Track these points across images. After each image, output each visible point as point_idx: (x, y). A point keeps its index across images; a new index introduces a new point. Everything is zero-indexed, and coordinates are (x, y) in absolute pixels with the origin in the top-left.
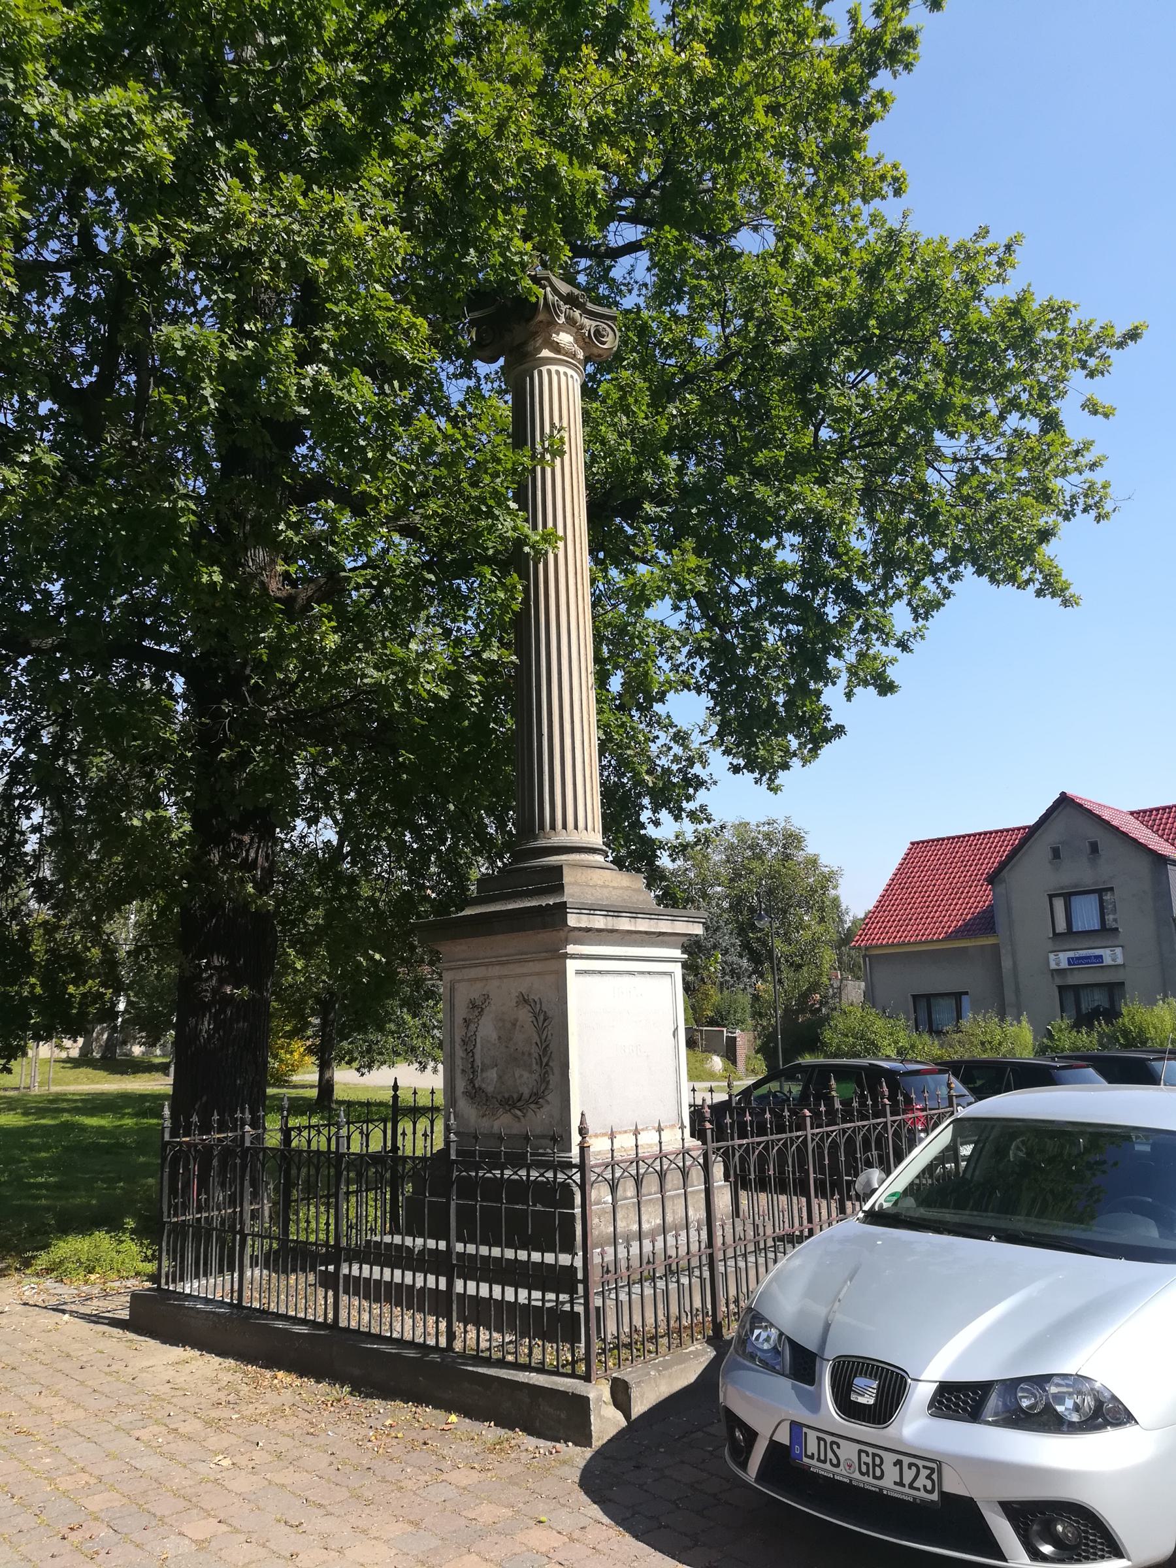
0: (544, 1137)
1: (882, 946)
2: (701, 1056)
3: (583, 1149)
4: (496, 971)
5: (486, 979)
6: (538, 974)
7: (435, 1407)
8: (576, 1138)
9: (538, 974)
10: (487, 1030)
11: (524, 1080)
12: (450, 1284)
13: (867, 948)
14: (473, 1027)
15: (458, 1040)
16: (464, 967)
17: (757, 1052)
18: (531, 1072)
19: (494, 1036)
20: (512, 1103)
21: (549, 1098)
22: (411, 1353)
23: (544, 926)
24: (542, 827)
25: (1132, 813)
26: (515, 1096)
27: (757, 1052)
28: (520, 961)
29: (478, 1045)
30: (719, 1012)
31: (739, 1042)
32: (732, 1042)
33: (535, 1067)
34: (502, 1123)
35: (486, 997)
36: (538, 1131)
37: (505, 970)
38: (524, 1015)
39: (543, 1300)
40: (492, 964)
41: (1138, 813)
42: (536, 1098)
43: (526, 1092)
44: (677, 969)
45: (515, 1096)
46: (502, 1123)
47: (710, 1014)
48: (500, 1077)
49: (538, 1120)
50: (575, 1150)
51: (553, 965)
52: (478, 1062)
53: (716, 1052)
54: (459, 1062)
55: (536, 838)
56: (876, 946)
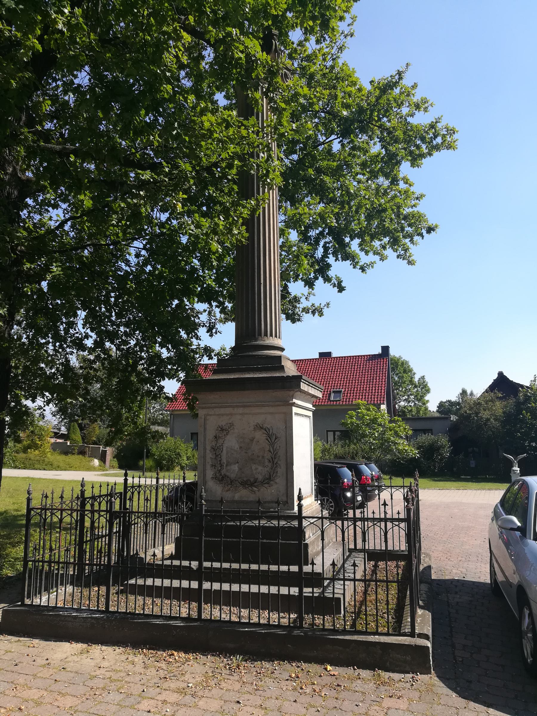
0: (272, 502)
1: (180, 410)
2: (87, 459)
3: (300, 506)
4: (240, 410)
5: (231, 414)
6: (271, 413)
7: (186, 652)
8: (296, 503)
9: (271, 413)
10: (231, 442)
11: (259, 471)
12: (200, 585)
13: (172, 411)
14: (220, 441)
15: (208, 448)
16: (216, 407)
17: (114, 458)
18: (264, 467)
19: (237, 446)
20: (249, 484)
21: (277, 480)
22: (279, 632)
23: (283, 388)
24: (260, 334)
25: (292, 361)
26: (252, 480)
27: (114, 458)
28: (258, 406)
29: (225, 451)
30: (98, 438)
31: (108, 453)
32: (104, 453)
33: (267, 463)
34: (242, 494)
35: (232, 425)
36: (269, 498)
37: (247, 410)
38: (260, 436)
39: (313, 593)
40: (237, 407)
41: (295, 361)
42: (268, 480)
43: (260, 478)
44: (310, 414)
45: (252, 480)
46: (242, 494)
47: (94, 439)
48: (240, 469)
49: (268, 493)
50: (296, 508)
51: (283, 409)
52: (224, 461)
53: (95, 457)
54: (208, 460)
55: (256, 340)
56: (177, 410)
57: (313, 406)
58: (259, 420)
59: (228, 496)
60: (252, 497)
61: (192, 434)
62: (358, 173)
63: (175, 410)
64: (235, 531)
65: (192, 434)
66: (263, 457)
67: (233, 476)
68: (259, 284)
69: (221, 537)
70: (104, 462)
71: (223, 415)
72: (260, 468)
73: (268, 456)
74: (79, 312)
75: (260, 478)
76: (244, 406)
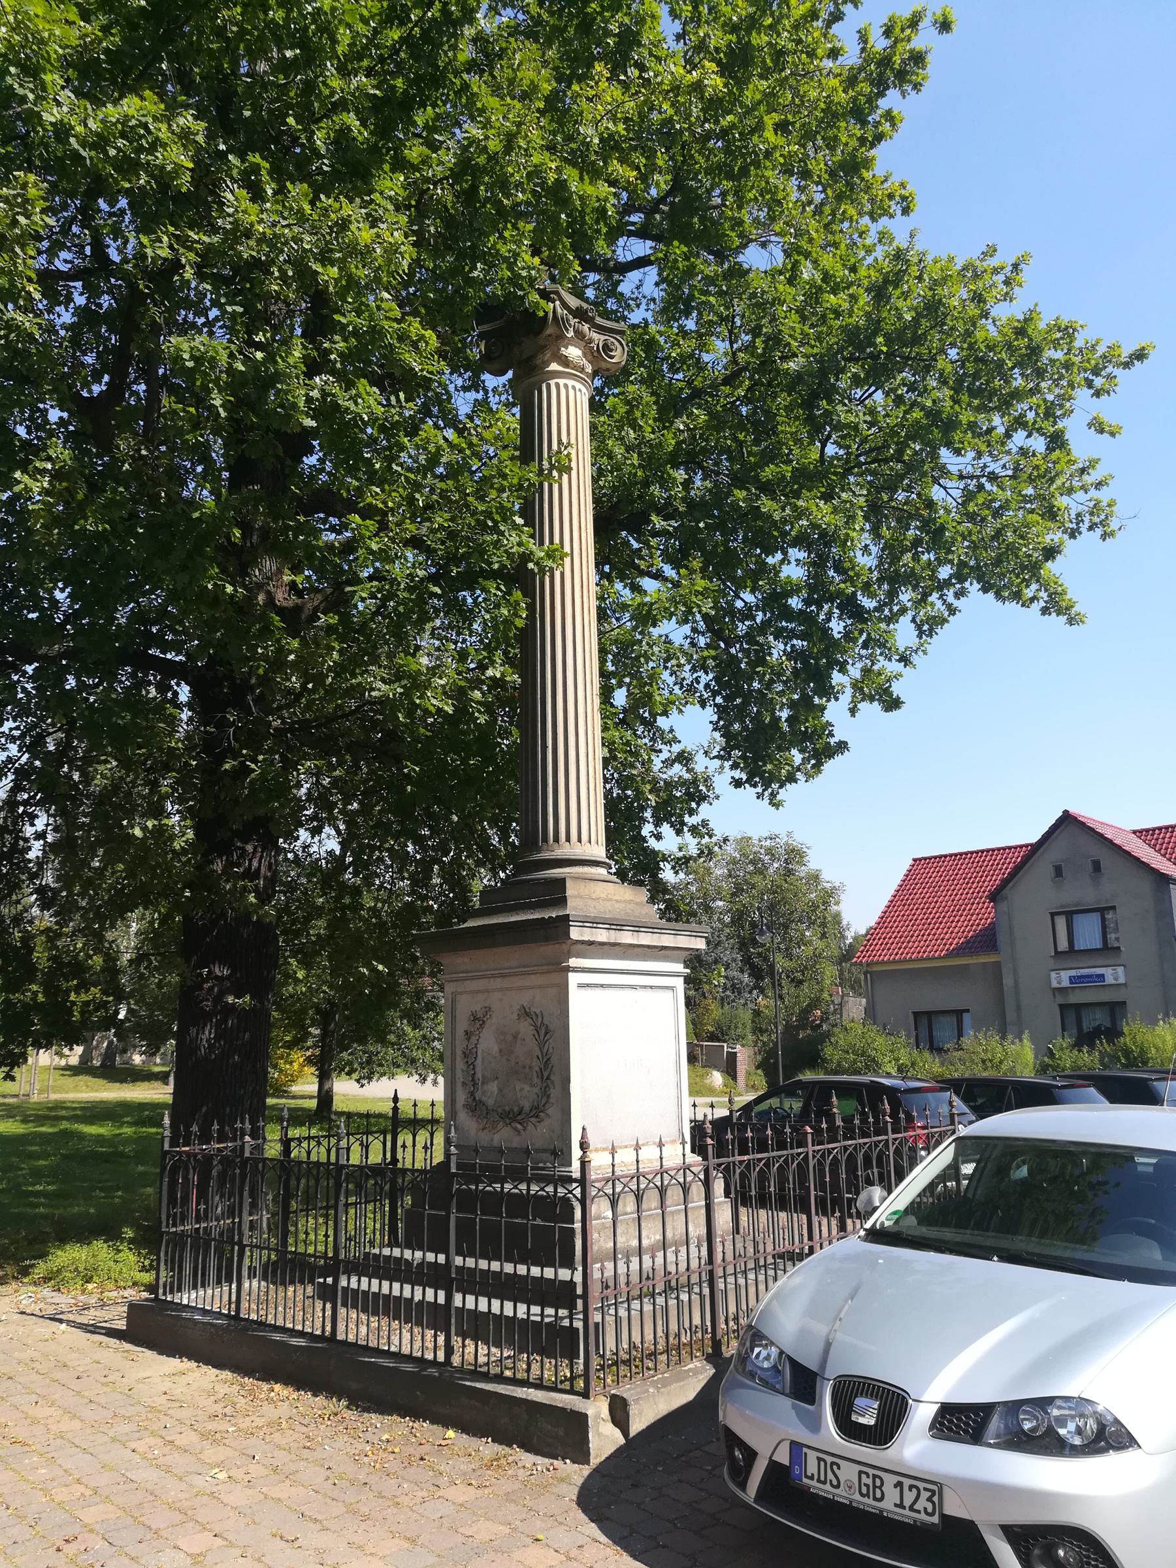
0: (544, 1151)
1: (883, 962)
2: (701, 1071)
3: (584, 1164)
4: (498, 983)
5: (487, 991)
6: (540, 987)
8: (576, 1153)
9: (540, 987)
10: (488, 1043)
11: (526, 1094)
13: (868, 965)
14: (474, 1040)
15: (459, 1053)
17: (757, 1068)
18: (532, 1086)
19: (496, 1049)
21: (549, 1111)
23: (547, 939)
24: (545, 840)
25: (1134, 832)
27: (757, 1068)
30: (719, 1027)
31: (740, 1057)
32: (732, 1057)
33: (536, 1080)
34: (504, 1136)
35: (488, 1010)
36: (539, 1144)
40: (493, 976)
41: (1141, 831)
42: (537, 1111)
43: (527, 1106)
44: (679, 983)
45: (516, 1109)
46: (504, 1136)
47: (711, 1029)
48: (500, 1090)
49: (538, 1134)
51: (555, 978)
52: (479, 1075)
54: (459, 1074)
55: (539, 850)
56: (878, 963)
57: (686, 967)
58: (524, 999)
59: (485, 1138)
60: (516, 1142)
61: (916, 1015)
62: (846, 468)
63: (872, 964)
64: (494, 1202)
65: (916, 1015)
66: (531, 1067)
67: (490, 1102)
68: (545, 747)
69: (526, 1217)
70: (734, 1078)
71: (478, 992)
72: (527, 1088)
73: (536, 1065)
74: (328, 830)
75: (527, 1106)
76: (503, 976)
